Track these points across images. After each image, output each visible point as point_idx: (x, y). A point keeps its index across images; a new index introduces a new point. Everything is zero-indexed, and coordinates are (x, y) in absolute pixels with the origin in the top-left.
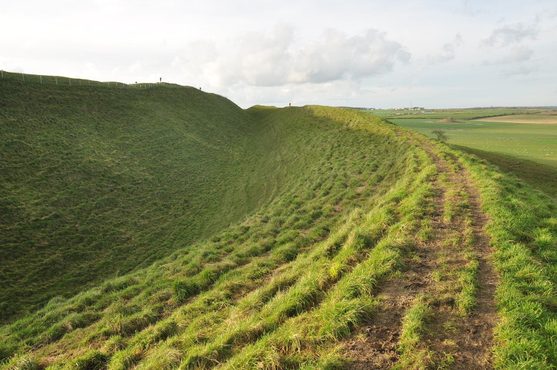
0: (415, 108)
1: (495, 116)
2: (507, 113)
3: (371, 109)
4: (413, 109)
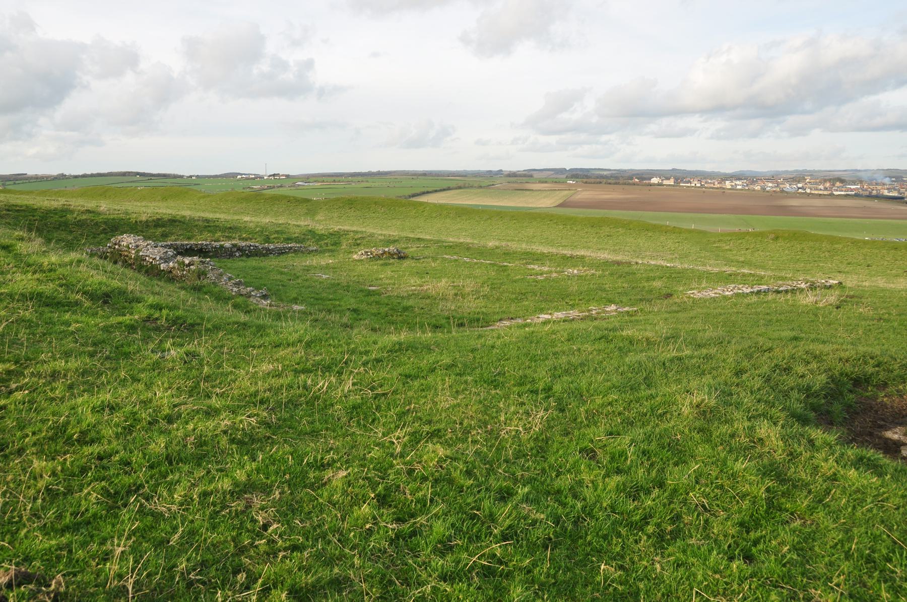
0: (274, 175)
1: (436, 191)
3: (191, 177)
4: (272, 178)
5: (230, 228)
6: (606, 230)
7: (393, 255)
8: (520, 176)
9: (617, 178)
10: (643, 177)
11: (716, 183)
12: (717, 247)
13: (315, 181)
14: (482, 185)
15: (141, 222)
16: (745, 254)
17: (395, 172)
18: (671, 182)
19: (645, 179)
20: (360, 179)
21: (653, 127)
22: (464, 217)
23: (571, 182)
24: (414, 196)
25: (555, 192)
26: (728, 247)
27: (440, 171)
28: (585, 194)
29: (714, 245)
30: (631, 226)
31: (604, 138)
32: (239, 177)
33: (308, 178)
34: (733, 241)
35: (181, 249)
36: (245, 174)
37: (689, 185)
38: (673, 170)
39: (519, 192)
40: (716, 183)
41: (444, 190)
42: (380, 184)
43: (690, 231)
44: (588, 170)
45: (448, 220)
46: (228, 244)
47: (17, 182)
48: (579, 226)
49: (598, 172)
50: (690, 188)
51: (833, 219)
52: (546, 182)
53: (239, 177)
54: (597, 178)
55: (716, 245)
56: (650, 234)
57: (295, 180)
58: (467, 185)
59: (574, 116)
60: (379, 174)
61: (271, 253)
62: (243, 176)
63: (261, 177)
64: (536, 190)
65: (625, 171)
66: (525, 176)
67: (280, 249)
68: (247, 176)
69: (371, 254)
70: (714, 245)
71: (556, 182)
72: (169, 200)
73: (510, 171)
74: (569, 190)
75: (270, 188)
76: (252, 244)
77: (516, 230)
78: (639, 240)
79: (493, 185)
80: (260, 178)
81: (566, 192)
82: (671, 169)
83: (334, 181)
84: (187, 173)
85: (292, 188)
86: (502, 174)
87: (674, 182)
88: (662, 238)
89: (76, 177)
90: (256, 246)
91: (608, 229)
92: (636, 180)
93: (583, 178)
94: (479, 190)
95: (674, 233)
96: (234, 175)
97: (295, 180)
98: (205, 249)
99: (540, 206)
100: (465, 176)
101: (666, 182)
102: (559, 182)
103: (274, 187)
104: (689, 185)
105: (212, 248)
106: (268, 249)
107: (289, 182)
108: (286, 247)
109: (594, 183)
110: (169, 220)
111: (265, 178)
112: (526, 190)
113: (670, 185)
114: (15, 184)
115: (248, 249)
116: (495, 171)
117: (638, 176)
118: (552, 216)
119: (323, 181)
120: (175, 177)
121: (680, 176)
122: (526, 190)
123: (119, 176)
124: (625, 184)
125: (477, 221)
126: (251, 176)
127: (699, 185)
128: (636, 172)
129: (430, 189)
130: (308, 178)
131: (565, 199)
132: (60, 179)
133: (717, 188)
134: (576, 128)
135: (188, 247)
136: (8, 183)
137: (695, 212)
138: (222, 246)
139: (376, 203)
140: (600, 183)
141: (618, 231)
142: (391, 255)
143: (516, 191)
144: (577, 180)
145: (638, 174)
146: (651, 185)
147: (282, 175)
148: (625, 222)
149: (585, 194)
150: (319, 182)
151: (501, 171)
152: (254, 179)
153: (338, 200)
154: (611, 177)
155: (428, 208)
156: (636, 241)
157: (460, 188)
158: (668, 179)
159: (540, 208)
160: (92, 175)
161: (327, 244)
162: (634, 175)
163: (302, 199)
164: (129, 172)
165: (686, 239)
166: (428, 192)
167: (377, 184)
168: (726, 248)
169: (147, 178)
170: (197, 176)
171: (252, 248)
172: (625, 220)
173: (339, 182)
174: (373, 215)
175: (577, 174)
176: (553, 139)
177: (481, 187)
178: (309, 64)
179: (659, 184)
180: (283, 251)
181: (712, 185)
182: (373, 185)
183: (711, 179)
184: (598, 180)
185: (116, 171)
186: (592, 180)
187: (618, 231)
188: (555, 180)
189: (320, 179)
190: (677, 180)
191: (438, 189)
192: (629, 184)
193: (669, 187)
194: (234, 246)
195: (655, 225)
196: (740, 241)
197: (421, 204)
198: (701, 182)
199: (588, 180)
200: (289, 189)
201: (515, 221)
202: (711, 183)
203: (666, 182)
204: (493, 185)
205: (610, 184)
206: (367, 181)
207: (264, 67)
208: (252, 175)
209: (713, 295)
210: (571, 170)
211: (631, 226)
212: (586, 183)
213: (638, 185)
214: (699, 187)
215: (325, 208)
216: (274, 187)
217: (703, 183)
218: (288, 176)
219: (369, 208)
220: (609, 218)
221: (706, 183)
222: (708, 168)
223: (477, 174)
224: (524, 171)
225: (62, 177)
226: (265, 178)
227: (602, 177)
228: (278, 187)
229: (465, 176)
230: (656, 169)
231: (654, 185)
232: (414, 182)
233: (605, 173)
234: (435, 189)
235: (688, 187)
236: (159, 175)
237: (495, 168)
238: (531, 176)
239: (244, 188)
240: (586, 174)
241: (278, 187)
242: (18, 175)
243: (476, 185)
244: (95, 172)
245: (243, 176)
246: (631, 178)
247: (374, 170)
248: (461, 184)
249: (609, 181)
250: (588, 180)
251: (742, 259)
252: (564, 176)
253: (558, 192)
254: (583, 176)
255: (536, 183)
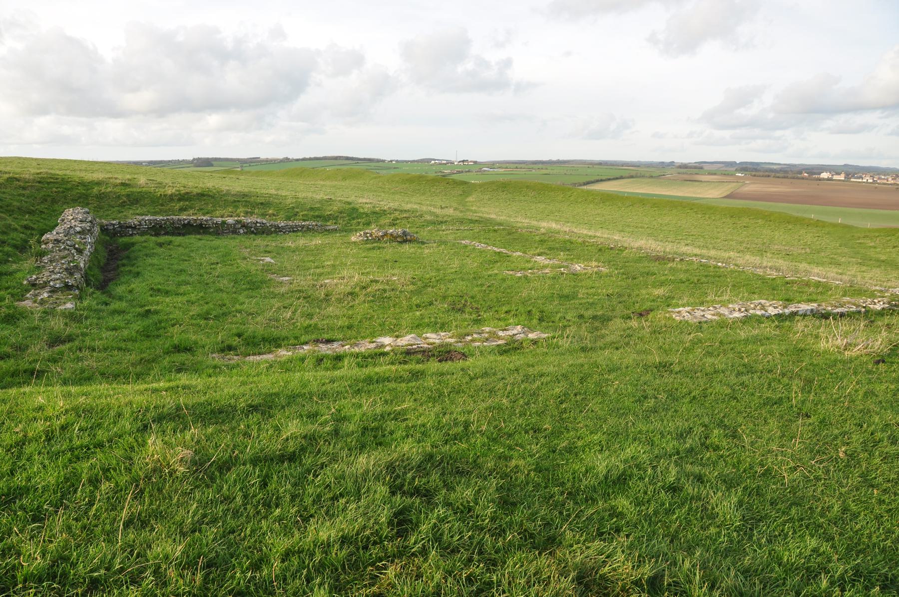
0: (463, 161)
1: (609, 180)
2: (624, 175)
3: (391, 161)
4: (462, 163)
5: (262, 204)
6: (745, 221)
7: (397, 237)
8: (691, 167)
9: (786, 172)
10: (813, 171)
11: (890, 179)
12: (860, 243)
13: (499, 168)
14: (654, 175)
15: (165, 195)
16: (890, 252)
17: (573, 161)
18: (842, 177)
19: (815, 174)
20: (540, 166)
21: (829, 123)
22: (607, 203)
23: (740, 175)
24: (588, 183)
25: (723, 183)
26: (872, 244)
27: (615, 162)
28: (752, 187)
29: (858, 241)
30: (772, 218)
31: (778, 133)
32: (433, 162)
33: (493, 165)
34: (880, 238)
35: (178, 224)
36: (438, 160)
37: (860, 180)
38: (845, 165)
39: (688, 182)
40: (890, 179)
41: (617, 179)
42: (558, 171)
43: (835, 225)
44: (758, 164)
45: (591, 206)
46: (230, 221)
47: (252, 164)
48: (718, 216)
49: (768, 166)
50: (861, 184)
51: (747, 202)
52: (715, 174)
53: (433, 162)
54: (767, 171)
55: (860, 241)
56: (790, 227)
57: (481, 166)
58: (639, 175)
59: (753, 111)
60: (559, 162)
61: (281, 231)
62: (437, 161)
63: (452, 163)
64: (705, 182)
65: (795, 166)
66: (695, 168)
67: (292, 227)
68: (440, 162)
69: (371, 235)
70: (858, 241)
71: (725, 174)
72: (347, 180)
73: (682, 163)
74: (737, 182)
75: (459, 172)
76: (258, 221)
77: (653, 217)
78: (776, 233)
79: (664, 175)
80: (451, 163)
81: (735, 184)
82: (843, 164)
83: (517, 168)
84: (388, 158)
85: (478, 173)
86: (674, 165)
87: (845, 178)
88: (802, 232)
89: (297, 160)
90: (263, 223)
91: (747, 220)
92: (806, 174)
93: (752, 171)
94: (650, 180)
95: (817, 226)
96: (428, 161)
97: (481, 166)
98: (206, 225)
99: (707, 196)
100: (639, 166)
101: (835, 177)
102: (728, 175)
103: (462, 172)
104: (860, 180)
105: (213, 223)
106: (277, 227)
107: (477, 167)
108: (299, 225)
109: (763, 176)
110: (198, 194)
111: (456, 163)
112: (695, 181)
113: (840, 180)
114: (250, 166)
115: (254, 225)
116: (666, 163)
117: (807, 171)
118: (693, 204)
119: (507, 168)
120: (378, 161)
121: (851, 172)
122: (695, 181)
123: (331, 159)
124: (794, 178)
125: (619, 207)
126: (443, 162)
127: (871, 181)
128: (806, 167)
129: (604, 178)
130: (493, 165)
131: (732, 190)
132: (284, 162)
133: (891, 184)
134: (751, 124)
135: (186, 222)
136: (245, 165)
137: (788, 202)
138: (224, 223)
139: (527, 187)
140: (769, 176)
141: (757, 223)
142: (394, 238)
143: (686, 182)
144: (746, 173)
145: (808, 169)
146: (820, 180)
147: (471, 161)
148: (766, 214)
149: (752, 187)
150: (503, 168)
151: (673, 162)
152: (445, 164)
153: (493, 183)
154: (781, 170)
155: (575, 194)
156: (773, 233)
157: (632, 177)
158: (838, 174)
159: (707, 198)
160: (310, 159)
161: (359, 223)
162: (804, 169)
163: (460, 181)
164: (340, 157)
165: (828, 233)
166: (602, 180)
167: (555, 172)
168: (871, 245)
169: (355, 162)
170: (397, 161)
171: (258, 225)
172: (766, 211)
173: (521, 168)
174: (523, 198)
175: (746, 168)
176: (727, 134)
177: (651, 177)
178: (508, 63)
179: (828, 179)
180: (295, 229)
181: (885, 181)
182: (551, 172)
183: (885, 175)
184: (767, 173)
185: (330, 155)
186: (761, 174)
187: (757, 223)
188: (724, 172)
189: (504, 166)
190: (848, 175)
191: (612, 177)
192: (798, 178)
193: (839, 182)
194: (238, 222)
195: (797, 218)
196: (889, 238)
197: (588, 192)
198: (874, 178)
199: (757, 173)
200: (475, 174)
201: (656, 209)
202: (884, 179)
203: (835, 177)
204: (664, 175)
205: (778, 177)
206: (547, 169)
207: (470, 65)
208: (444, 160)
209: (426, 346)
210: (741, 163)
211: (772, 218)
212: (755, 176)
213: (807, 179)
214: (870, 183)
215: (479, 190)
216: (462, 172)
217: (875, 179)
218: (475, 162)
219: (521, 192)
220: (750, 209)
221: (879, 178)
222: (883, 164)
223: (650, 165)
224: (695, 163)
225: (287, 160)
226: (456, 163)
227: (772, 171)
228: (466, 172)
229: (639, 166)
230: (827, 164)
231: (824, 179)
232: (589, 170)
233: (775, 167)
234: (609, 177)
235: (859, 182)
236: (365, 159)
237: (667, 160)
238: (702, 168)
239: (436, 172)
240: (755, 167)
241: (466, 172)
242: (254, 158)
243: (647, 175)
244: (312, 156)
245: (437, 161)
246: (801, 173)
247: (554, 159)
248: (633, 173)
249: (778, 175)
250: (757, 173)
251: (883, 258)
252: (734, 169)
253: (726, 184)
254: (753, 170)
255: (705, 174)
